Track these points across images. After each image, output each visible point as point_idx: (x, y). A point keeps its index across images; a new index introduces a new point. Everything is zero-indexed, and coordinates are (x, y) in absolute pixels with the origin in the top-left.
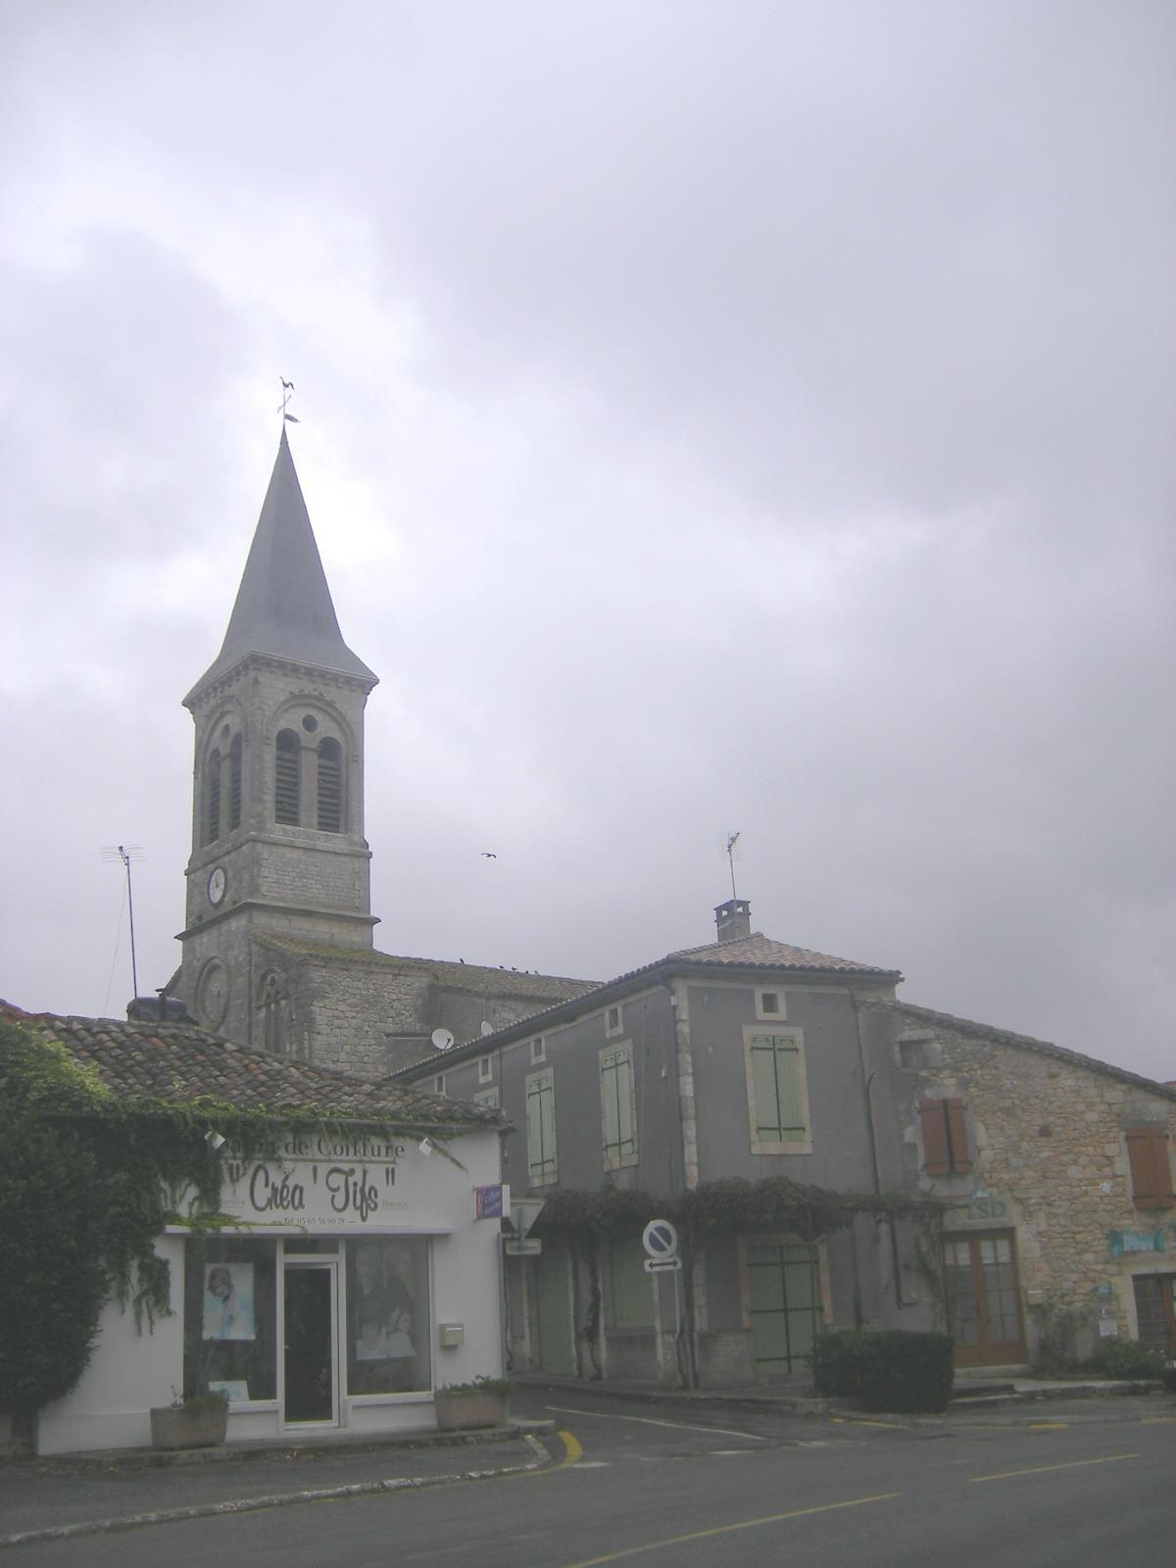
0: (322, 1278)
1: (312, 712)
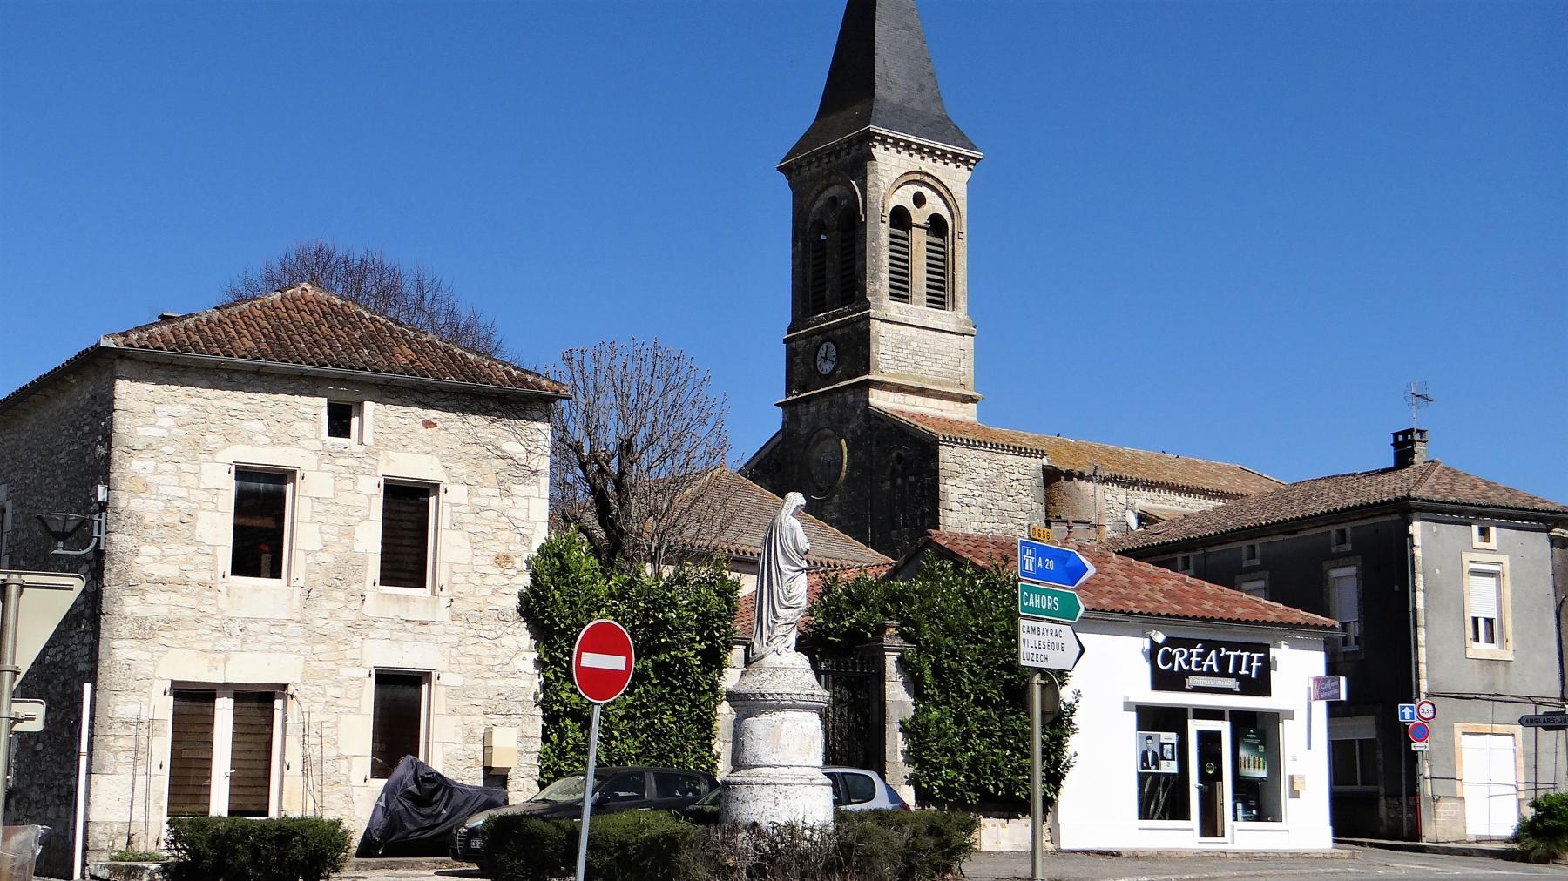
0: (1216, 736)
1: (924, 190)
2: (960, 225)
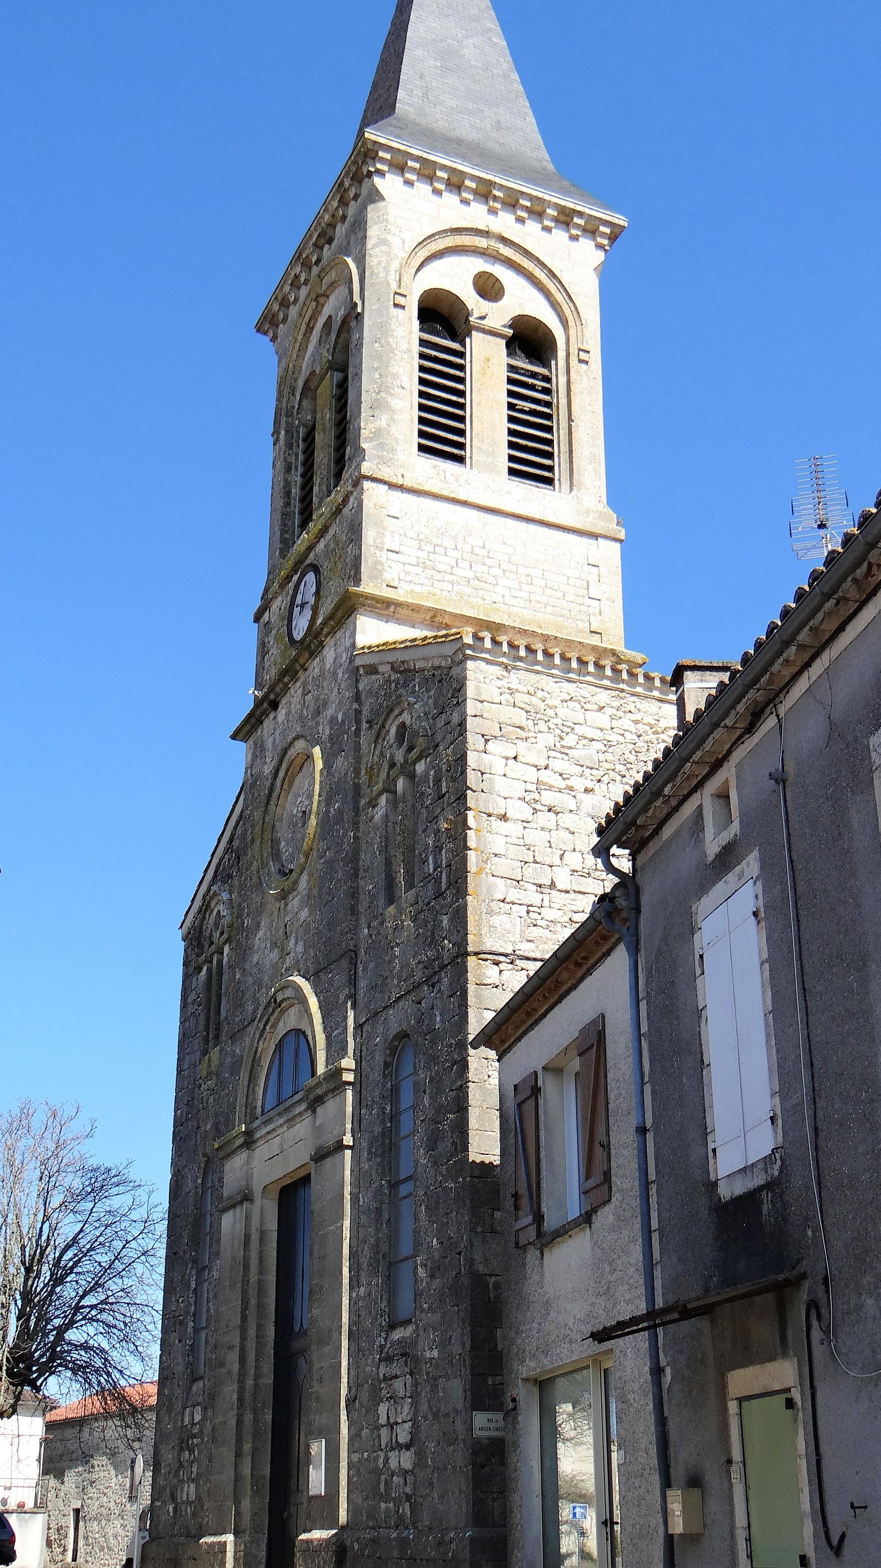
1: (499, 271)
2: (582, 338)
